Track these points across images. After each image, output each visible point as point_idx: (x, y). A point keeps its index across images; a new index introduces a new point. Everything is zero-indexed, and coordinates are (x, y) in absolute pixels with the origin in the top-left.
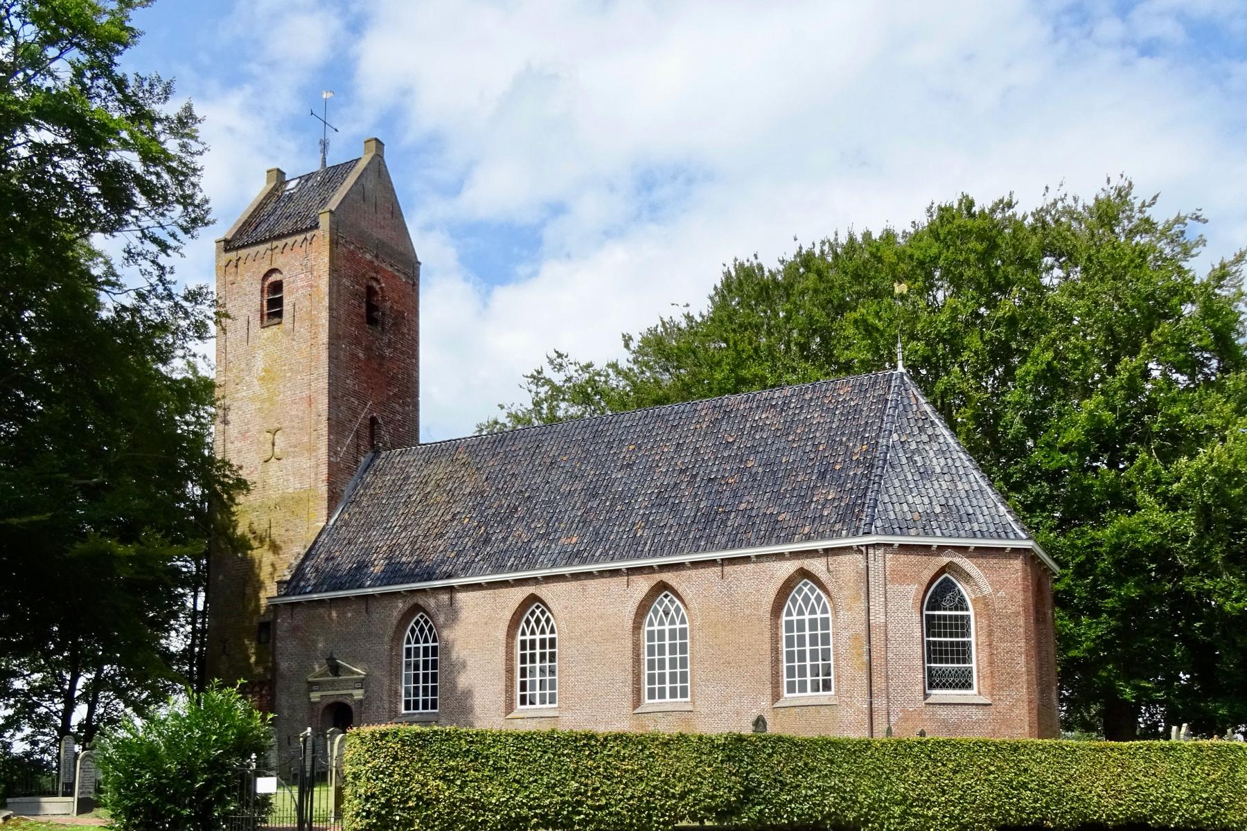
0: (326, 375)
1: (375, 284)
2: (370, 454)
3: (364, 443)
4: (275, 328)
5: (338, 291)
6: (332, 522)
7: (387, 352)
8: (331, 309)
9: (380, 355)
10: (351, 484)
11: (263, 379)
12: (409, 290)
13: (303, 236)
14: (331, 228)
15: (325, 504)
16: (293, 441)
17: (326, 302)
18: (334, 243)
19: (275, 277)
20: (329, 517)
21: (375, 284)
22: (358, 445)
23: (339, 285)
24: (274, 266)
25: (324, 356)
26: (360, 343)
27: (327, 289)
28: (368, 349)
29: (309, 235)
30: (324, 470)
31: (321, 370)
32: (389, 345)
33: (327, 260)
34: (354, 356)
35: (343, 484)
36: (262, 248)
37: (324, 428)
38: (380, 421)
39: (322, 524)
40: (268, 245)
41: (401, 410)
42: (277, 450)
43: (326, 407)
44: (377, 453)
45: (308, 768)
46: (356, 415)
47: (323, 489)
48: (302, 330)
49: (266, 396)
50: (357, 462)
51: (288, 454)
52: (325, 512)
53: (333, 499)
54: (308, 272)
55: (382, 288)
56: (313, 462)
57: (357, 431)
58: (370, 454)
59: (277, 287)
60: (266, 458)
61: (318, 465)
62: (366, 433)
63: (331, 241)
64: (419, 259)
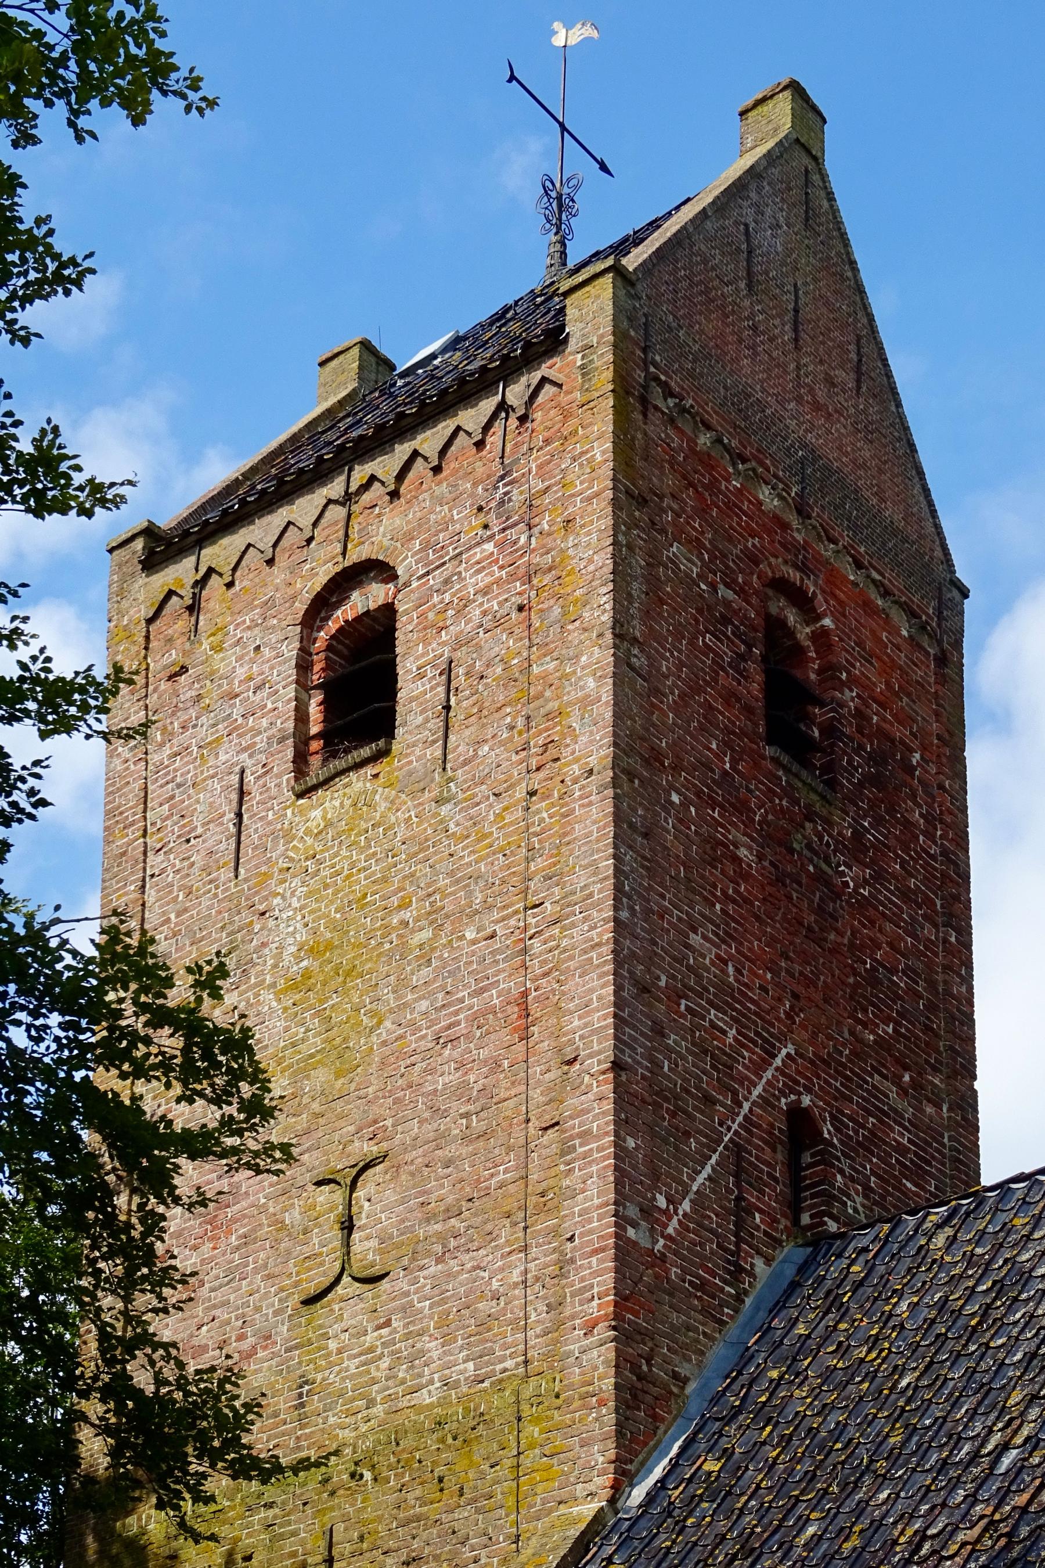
0: (603, 891)
1: (792, 617)
2: (791, 1253)
3: (767, 1200)
4: (358, 782)
5: (653, 584)
6: (638, 1494)
7: (850, 876)
8: (621, 634)
9: (820, 878)
10: (718, 1354)
11: (301, 983)
12: (925, 673)
13: (488, 405)
14: (619, 334)
15: (604, 1420)
16: (443, 1191)
17: (600, 611)
18: (633, 395)
19: (369, 597)
20: (624, 1477)
21: (792, 617)
22: (741, 1211)
23: (654, 560)
24: (355, 556)
25: (593, 818)
26: (742, 808)
27: (604, 561)
28: (774, 838)
29: (516, 393)
30: (596, 1278)
31: (580, 879)
32: (856, 848)
33: (602, 451)
34: (718, 853)
35: (683, 1350)
36: (303, 509)
37: (593, 1107)
38: (827, 1130)
39: (588, 1510)
40: (335, 488)
41: (856, 1529)
42: (364, 1245)
43: (603, 1018)
44: (820, 1244)
45: (681, 1488)
46: (731, 1083)
47: (593, 1359)
48: (488, 750)
49: (316, 1042)
50: (737, 1273)
51: (414, 1254)
52: (601, 1455)
53: (641, 1403)
54: (517, 574)
55: (821, 637)
56: (542, 1257)
57: (737, 1149)
58: (791, 1253)
59: (377, 634)
60: (312, 1288)
61: (564, 1265)
62: (770, 1162)
63: (622, 387)
64: (962, 574)
